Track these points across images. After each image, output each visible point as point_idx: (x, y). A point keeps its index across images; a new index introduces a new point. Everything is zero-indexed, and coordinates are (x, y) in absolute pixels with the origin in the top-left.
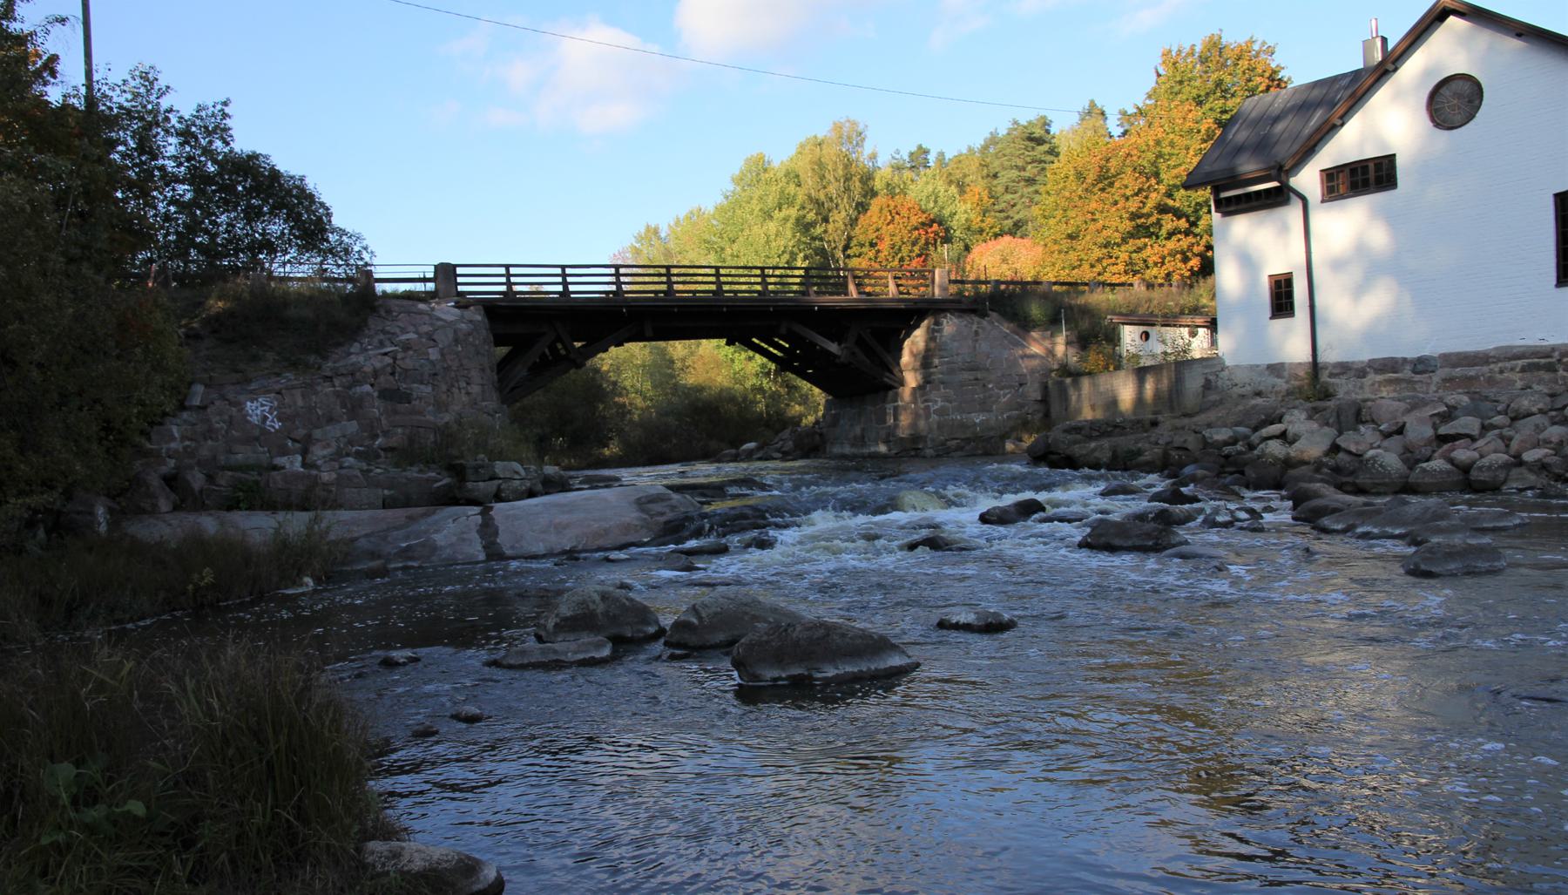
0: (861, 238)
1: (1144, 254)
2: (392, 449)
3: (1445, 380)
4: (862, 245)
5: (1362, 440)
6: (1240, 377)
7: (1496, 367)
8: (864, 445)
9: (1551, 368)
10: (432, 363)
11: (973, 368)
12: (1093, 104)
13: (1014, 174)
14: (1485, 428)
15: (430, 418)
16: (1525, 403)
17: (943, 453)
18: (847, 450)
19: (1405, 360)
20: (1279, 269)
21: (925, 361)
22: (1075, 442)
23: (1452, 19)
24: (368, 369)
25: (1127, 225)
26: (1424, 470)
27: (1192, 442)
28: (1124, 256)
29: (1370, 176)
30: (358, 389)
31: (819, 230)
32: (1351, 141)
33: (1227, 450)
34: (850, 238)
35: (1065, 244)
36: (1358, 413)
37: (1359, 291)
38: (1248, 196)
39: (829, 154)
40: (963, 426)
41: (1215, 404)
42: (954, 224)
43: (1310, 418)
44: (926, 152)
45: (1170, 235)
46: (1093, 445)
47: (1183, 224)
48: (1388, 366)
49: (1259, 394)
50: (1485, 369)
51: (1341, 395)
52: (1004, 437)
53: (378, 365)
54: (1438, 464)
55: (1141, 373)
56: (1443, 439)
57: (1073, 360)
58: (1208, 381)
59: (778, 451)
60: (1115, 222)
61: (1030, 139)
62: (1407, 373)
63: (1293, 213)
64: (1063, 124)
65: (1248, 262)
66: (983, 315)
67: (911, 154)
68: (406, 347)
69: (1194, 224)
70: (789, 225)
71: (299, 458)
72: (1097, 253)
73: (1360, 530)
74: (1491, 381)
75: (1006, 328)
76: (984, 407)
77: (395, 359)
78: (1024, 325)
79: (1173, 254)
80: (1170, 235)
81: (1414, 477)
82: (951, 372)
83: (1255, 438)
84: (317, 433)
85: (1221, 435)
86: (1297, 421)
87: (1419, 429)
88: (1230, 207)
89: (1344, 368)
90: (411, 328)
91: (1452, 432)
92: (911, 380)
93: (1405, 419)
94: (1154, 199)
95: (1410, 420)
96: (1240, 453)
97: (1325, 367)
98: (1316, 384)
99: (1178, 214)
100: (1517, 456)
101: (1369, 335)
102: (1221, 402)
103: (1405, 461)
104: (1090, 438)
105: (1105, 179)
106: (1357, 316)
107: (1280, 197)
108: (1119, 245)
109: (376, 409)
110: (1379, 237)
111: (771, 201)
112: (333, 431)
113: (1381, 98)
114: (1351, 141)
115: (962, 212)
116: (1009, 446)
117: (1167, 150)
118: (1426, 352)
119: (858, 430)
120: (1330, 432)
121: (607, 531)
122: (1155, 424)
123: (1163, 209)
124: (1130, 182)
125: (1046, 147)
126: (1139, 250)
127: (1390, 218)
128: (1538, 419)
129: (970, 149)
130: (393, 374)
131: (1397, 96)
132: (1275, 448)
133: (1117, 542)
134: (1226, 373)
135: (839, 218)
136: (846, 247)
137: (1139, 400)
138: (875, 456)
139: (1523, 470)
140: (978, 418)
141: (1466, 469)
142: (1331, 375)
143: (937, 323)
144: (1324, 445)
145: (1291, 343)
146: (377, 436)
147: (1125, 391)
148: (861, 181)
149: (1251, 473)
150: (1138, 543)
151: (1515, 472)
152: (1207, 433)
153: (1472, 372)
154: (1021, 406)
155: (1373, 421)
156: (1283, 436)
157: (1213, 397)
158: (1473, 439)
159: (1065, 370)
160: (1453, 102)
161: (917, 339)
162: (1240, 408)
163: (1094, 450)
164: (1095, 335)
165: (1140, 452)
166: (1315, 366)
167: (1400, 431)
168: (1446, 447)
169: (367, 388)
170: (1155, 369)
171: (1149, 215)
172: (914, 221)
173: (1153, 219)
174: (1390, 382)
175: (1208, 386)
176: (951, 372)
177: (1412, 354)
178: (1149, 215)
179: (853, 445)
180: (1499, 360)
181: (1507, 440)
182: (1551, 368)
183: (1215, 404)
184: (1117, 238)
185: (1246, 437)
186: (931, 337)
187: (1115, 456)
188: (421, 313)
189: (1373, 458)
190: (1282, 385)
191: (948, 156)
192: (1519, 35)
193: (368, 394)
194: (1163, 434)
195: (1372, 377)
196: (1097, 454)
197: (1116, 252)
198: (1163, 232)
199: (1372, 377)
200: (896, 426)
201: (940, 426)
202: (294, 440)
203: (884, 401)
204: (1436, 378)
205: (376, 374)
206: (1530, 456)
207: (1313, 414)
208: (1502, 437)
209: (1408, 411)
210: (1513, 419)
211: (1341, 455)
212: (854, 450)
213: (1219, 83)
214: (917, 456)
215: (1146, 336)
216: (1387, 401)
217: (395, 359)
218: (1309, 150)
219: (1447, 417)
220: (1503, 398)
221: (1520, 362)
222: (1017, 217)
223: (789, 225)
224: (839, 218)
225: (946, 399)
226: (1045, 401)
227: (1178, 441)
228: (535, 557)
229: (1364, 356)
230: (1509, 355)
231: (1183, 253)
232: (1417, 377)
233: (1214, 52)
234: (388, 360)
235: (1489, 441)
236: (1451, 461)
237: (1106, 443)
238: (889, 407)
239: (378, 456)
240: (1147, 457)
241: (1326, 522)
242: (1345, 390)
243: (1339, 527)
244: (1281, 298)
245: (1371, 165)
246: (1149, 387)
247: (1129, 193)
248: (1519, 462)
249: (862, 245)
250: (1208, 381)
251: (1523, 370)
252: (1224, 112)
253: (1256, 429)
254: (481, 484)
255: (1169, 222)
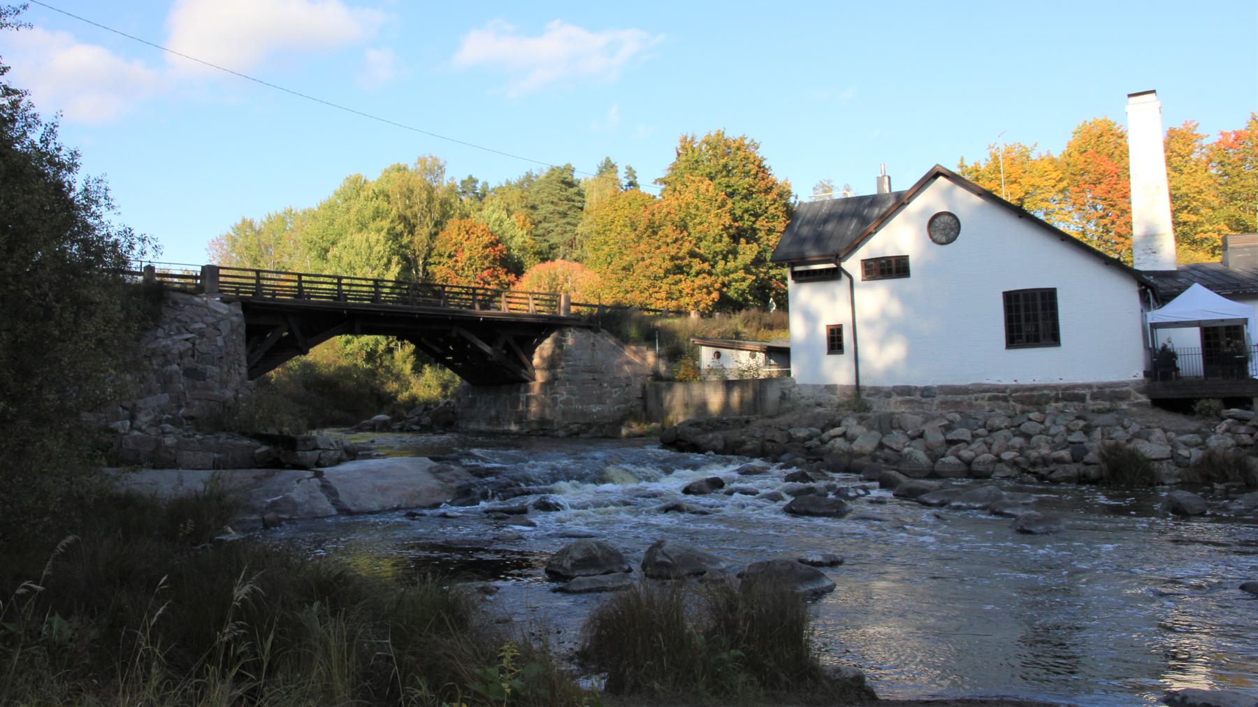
0: (442, 250)
1: (680, 286)
2: (192, 418)
3: (942, 403)
4: (441, 255)
5: (896, 440)
6: (806, 393)
7: (973, 397)
8: (499, 424)
9: (1005, 399)
10: (220, 349)
11: (591, 371)
12: (608, 160)
13: (552, 208)
14: (975, 436)
15: (217, 393)
16: (997, 422)
17: (573, 436)
18: (483, 427)
19: (916, 388)
20: (833, 322)
21: (551, 364)
22: (698, 434)
23: (941, 179)
24: (175, 352)
25: (668, 264)
26: (943, 463)
27: (778, 436)
28: (665, 287)
29: (890, 268)
30: (169, 368)
31: (406, 240)
32: (883, 243)
33: (808, 444)
34: (431, 250)
35: (621, 274)
36: (891, 422)
37: (882, 343)
38: (815, 271)
39: (416, 183)
40: (583, 414)
41: (788, 411)
42: (513, 245)
43: (859, 424)
44: (476, 181)
45: (698, 274)
46: (710, 436)
47: (706, 266)
48: (905, 391)
49: (819, 405)
50: (966, 397)
51: (875, 408)
52: (620, 422)
53: (182, 348)
54: (951, 459)
55: (729, 385)
56: (951, 443)
57: (662, 368)
58: (784, 394)
59: (417, 424)
60: (658, 261)
61: (563, 182)
62: (917, 397)
63: (841, 287)
64: (585, 173)
65: (810, 317)
66: (597, 331)
67: (463, 182)
68: (201, 334)
69: (713, 267)
70: (383, 233)
71: (128, 423)
72: (646, 283)
73: (954, 504)
74: (970, 405)
75: (612, 341)
76: (600, 401)
77: (194, 344)
78: (625, 340)
79: (700, 288)
80: (698, 274)
81: (938, 467)
82: (575, 372)
83: (825, 436)
84: (140, 403)
85: (802, 433)
86: (851, 425)
87: (935, 436)
88: (801, 277)
89: (877, 391)
90: (197, 319)
91: (955, 438)
92: (540, 377)
93: (923, 428)
94: (687, 247)
95: (927, 428)
96: (817, 446)
97: (865, 389)
98: (859, 399)
99: (704, 260)
100: (998, 456)
101: (889, 372)
102: (793, 409)
103: (929, 456)
104: (706, 431)
105: (653, 229)
106: (882, 359)
107: (834, 275)
108: (662, 278)
109: (181, 384)
110: (895, 308)
111: (368, 213)
112: (151, 401)
113: (897, 221)
114: (883, 243)
115: (519, 238)
116: (624, 431)
117: (693, 211)
118: (929, 384)
119: (493, 413)
120: (876, 434)
121: (419, 493)
122: (748, 422)
123: (693, 255)
124: (669, 231)
125: (575, 190)
126: (676, 283)
127: (904, 299)
128: (1005, 432)
129: (508, 183)
130: (193, 356)
131: (908, 219)
132: (840, 443)
133: (812, 509)
134: (795, 390)
135: (423, 233)
136: (429, 255)
137: (726, 405)
138: (508, 433)
139: (1002, 465)
140: (595, 409)
141: (969, 463)
142: (869, 395)
143: (563, 335)
144: (875, 444)
145: (838, 372)
146: (180, 407)
147: (715, 400)
148: (441, 205)
149: (828, 460)
150: (828, 510)
151: (999, 466)
152: (791, 431)
153: (958, 398)
154: (627, 401)
155: (900, 428)
156: (844, 435)
157: (787, 405)
158: (968, 443)
159: (657, 376)
160: (944, 228)
161: (546, 347)
162: (808, 414)
163: (712, 440)
164: (677, 352)
165: (744, 443)
166: (858, 387)
167: (921, 435)
168: (953, 448)
169: (175, 367)
170: (741, 383)
171: (683, 259)
172: (486, 239)
173: (686, 262)
174: (906, 402)
175: (783, 397)
176: (575, 372)
177: (921, 384)
178: (683, 259)
179: (489, 424)
180: (974, 392)
181: (989, 446)
182: (1005, 399)
183: (788, 411)
184: (661, 273)
185: (817, 435)
186: (559, 344)
187: (726, 445)
188: (197, 305)
189: (909, 453)
190: (836, 399)
191: (491, 186)
192: (980, 195)
193: (176, 372)
194: (756, 428)
195: (895, 398)
196: (714, 443)
197: (658, 283)
198: (693, 271)
199: (895, 398)
200: (528, 411)
201: (564, 414)
202: (125, 408)
203: (518, 390)
204: (937, 400)
205: (181, 355)
206: (1007, 456)
207: (861, 420)
208: (985, 443)
209: (925, 422)
210: (990, 431)
211: (886, 450)
212: (490, 428)
213: (725, 166)
214: (544, 435)
215: (718, 355)
216: (912, 420)
217: (194, 344)
218: (853, 247)
219: (948, 428)
220: (980, 417)
221: (988, 395)
222: (552, 241)
223: (383, 233)
224: (423, 233)
225: (570, 393)
226: (644, 398)
227: (768, 435)
228: (372, 513)
229: (888, 383)
230: (982, 389)
231: (707, 287)
232: (924, 400)
233: (720, 146)
234: (189, 345)
235: (978, 445)
236: (959, 457)
237: (720, 435)
238: (523, 397)
239: (181, 423)
240: (749, 446)
241: (925, 498)
242: (879, 407)
243: (935, 501)
244: (835, 341)
245: (893, 262)
246: (735, 397)
247: (669, 240)
248: (1000, 461)
249: (441, 255)
250: (784, 394)
251: (990, 399)
252: (728, 186)
253: (823, 431)
254: (308, 453)
255: (697, 265)
